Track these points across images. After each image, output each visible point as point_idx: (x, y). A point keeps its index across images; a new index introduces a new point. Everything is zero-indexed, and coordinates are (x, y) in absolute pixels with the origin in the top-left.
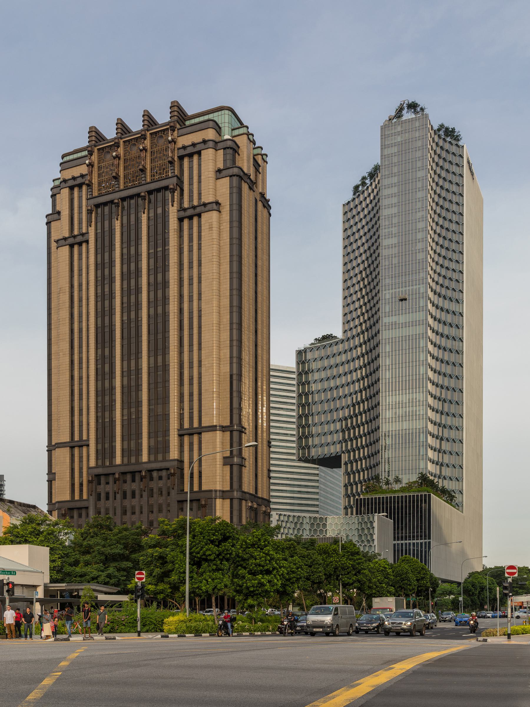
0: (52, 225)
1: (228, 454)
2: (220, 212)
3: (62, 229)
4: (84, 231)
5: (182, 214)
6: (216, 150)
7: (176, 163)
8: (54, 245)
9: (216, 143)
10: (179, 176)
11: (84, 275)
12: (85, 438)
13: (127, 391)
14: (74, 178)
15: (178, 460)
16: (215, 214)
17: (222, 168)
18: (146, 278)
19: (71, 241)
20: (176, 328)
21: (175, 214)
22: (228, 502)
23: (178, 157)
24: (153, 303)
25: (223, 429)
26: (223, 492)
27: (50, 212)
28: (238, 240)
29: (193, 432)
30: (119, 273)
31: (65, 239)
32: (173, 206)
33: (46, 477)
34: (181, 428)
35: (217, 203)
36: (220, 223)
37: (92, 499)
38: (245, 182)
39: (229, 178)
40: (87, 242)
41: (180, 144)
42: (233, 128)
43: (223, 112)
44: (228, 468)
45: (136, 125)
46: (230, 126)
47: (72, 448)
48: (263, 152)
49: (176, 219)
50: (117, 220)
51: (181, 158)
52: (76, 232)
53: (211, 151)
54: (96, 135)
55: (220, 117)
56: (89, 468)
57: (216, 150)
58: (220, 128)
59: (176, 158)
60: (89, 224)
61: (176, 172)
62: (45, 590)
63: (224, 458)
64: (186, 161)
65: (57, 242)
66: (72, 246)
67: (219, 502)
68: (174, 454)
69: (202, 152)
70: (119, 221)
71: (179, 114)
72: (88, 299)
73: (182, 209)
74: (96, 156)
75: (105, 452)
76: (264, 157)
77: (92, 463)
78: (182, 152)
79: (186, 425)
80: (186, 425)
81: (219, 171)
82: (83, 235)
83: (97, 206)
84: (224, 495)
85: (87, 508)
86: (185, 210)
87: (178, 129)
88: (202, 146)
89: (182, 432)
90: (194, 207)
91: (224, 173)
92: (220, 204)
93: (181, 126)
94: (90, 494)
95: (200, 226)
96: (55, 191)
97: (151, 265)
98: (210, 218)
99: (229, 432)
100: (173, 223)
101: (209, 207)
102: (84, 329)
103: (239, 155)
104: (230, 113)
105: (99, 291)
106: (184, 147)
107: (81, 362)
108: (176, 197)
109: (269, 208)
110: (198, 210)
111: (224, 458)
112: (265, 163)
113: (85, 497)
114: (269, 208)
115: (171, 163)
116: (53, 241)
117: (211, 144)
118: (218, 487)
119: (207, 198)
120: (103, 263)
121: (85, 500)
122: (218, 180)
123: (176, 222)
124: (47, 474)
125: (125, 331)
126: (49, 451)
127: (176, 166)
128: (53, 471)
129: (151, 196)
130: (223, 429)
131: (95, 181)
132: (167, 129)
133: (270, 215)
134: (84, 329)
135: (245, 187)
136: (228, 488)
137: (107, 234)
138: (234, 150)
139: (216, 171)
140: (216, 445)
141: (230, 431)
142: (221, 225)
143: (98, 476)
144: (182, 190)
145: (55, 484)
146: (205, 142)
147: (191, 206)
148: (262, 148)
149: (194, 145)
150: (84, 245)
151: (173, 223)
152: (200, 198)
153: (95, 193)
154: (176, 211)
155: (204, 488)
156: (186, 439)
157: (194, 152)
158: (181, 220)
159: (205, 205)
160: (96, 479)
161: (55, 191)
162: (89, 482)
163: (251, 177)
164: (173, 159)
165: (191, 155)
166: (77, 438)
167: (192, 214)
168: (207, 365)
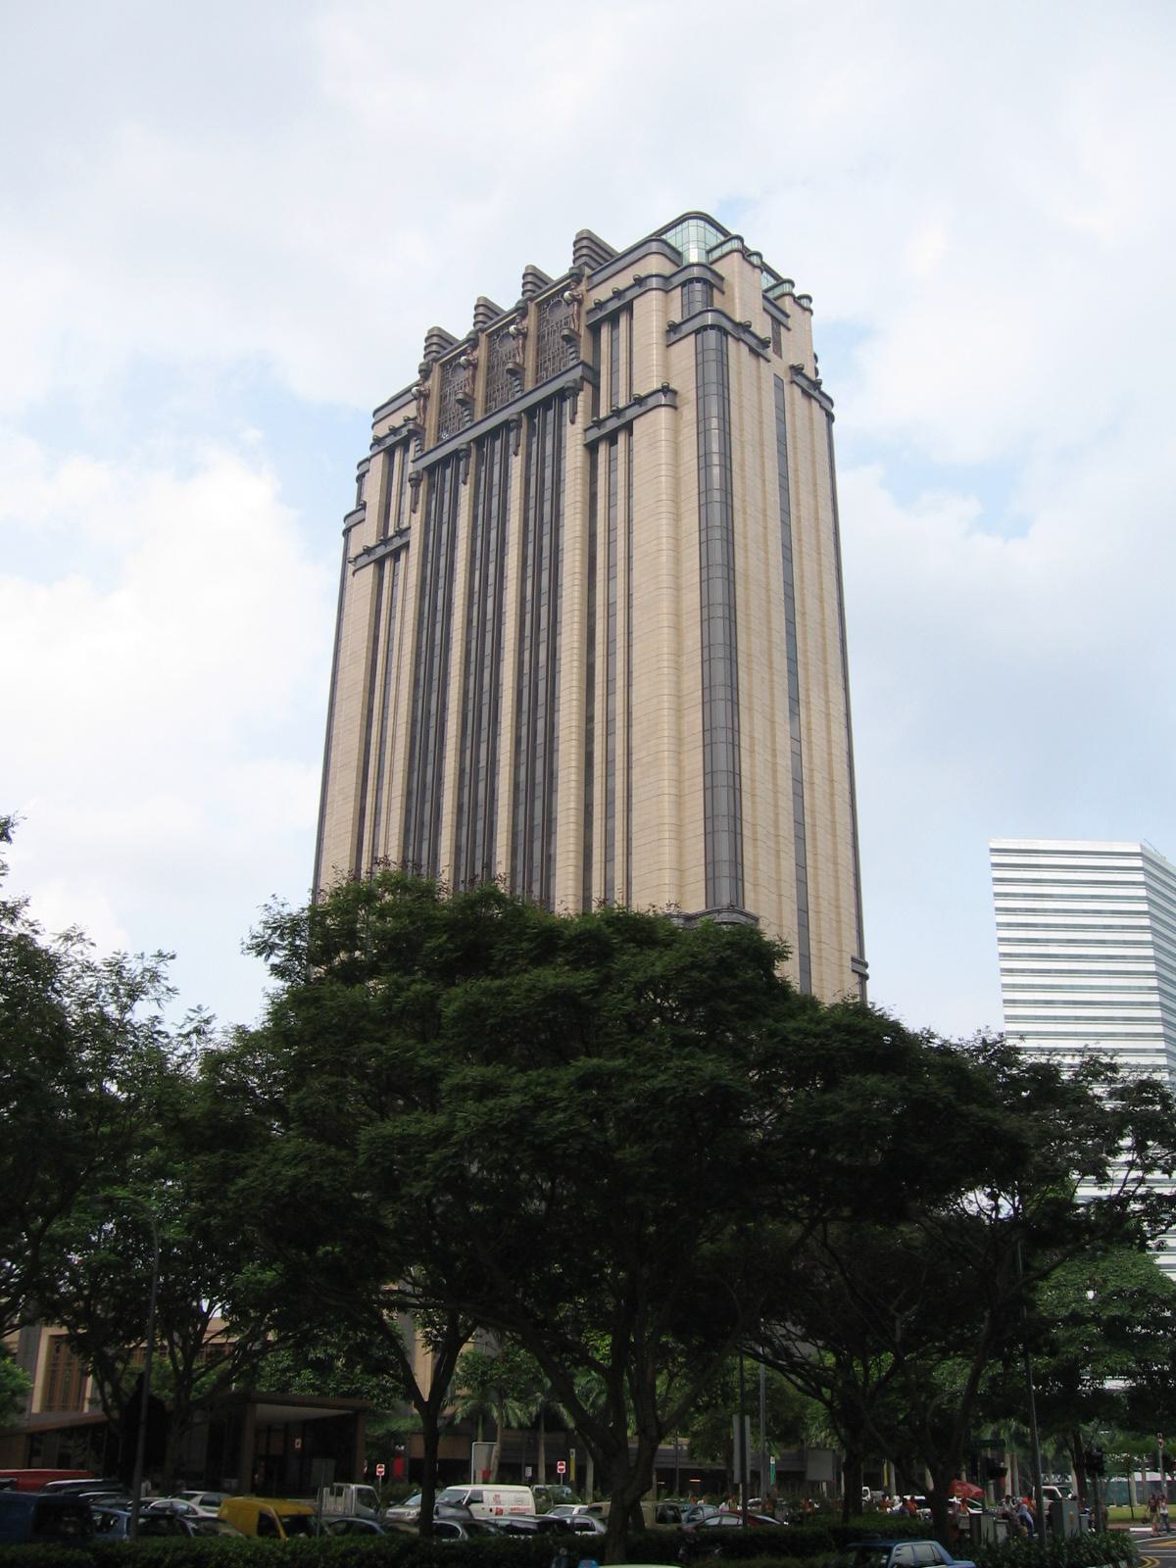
0: (375, 539)
3: (367, 535)
5: (594, 434)
6: (667, 292)
7: (582, 339)
14: (394, 431)
19: (381, 551)
21: (579, 436)
31: (368, 551)
32: (573, 422)
35: (666, 390)
36: (676, 431)
38: (738, 340)
42: (708, 248)
43: (685, 224)
45: (508, 298)
46: (702, 245)
47: (380, 563)
48: (797, 292)
49: (580, 448)
51: (595, 329)
54: (437, 341)
55: (679, 235)
57: (667, 292)
59: (583, 332)
61: (582, 355)
62: (501, 1481)
66: (380, 563)
70: (468, 486)
71: (591, 252)
76: (804, 302)
81: (673, 328)
83: (431, 469)
87: (589, 277)
88: (637, 291)
91: (686, 328)
92: (675, 393)
93: (593, 269)
96: (364, 468)
98: (653, 427)
101: (651, 402)
102: (619, 836)
104: (701, 223)
106: (600, 305)
108: (580, 404)
109: (826, 404)
112: (807, 313)
114: (826, 404)
115: (571, 340)
117: (654, 282)
119: (648, 382)
123: (579, 453)
133: (830, 417)
134: (619, 836)
138: (705, 281)
144: (596, 388)
146: (639, 281)
148: (793, 285)
149: (618, 294)
153: (430, 444)
157: (619, 310)
158: (591, 448)
159: (640, 401)
163: (756, 329)
165: (611, 439)
167: (611, 432)
168: (644, 760)
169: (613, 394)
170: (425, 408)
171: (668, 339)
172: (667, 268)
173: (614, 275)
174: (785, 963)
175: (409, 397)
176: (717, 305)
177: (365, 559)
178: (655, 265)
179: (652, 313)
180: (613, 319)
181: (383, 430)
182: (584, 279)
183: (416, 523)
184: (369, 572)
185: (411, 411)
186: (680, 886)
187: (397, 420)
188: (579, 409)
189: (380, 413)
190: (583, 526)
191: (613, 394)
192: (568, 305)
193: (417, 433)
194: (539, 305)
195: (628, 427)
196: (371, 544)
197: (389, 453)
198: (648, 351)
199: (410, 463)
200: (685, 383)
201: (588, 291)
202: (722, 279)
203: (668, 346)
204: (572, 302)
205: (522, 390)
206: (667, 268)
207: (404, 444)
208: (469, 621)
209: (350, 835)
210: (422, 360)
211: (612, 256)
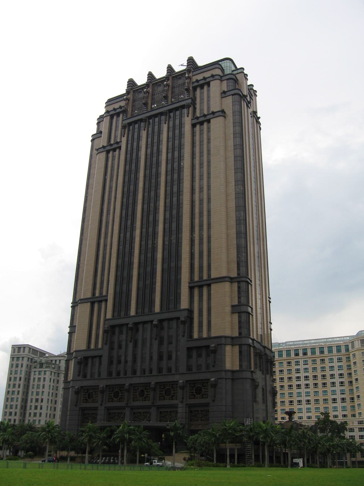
1: (236, 303)
2: (225, 117)
3: (103, 141)
4: (119, 140)
5: (195, 121)
8: (95, 152)
9: (221, 77)
10: (193, 98)
11: (108, 250)
12: (104, 294)
13: (146, 214)
14: (115, 109)
15: (188, 310)
16: (221, 119)
17: (226, 90)
18: (166, 133)
20: (188, 229)
22: (237, 349)
23: (192, 87)
24: (167, 232)
25: (231, 280)
26: (232, 338)
27: (95, 132)
28: (239, 127)
29: (202, 285)
30: (143, 176)
31: (104, 147)
32: (188, 116)
33: (68, 330)
34: (191, 280)
35: (223, 111)
37: (107, 347)
39: (231, 96)
40: (120, 148)
41: (194, 79)
43: (225, 61)
44: (236, 316)
47: (108, 152)
49: (187, 287)
50: (144, 130)
51: (195, 89)
52: (112, 142)
53: (218, 82)
54: (131, 83)
56: (106, 320)
58: (224, 70)
59: (191, 88)
60: (122, 135)
63: (233, 306)
64: (198, 90)
65: (97, 150)
66: (108, 152)
67: (228, 348)
68: (184, 304)
69: (212, 285)
70: (146, 131)
72: (115, 198)
73: (195, 117)
74: (132, 95)
75: (121, 302)
77: (109, 315)
78: (196, 84)
79: (196, 278)
80: (196, 278)
81: (224, 92)
82: (117, 143)
83: (130, 124)
84: (233, 341)
85: (100, 357)
86: (197, 118)
87: (193, 72)
88: (212, 116)
89: (192, 285)
90: (205, 116)
91: (228, 94)
94: (105, 343)
95: (209, 295)
97: (168, 168)
98: (216, 123)
99: (238, 347)
100: (187, 128)
103: (238, 84)
105: (126, 189)
106: (197, 81)
107: (108, 210)
108: (186, 328)
110: (208, 117)
111: (233, 306)
113: (100, 346)
116: (94, 149)
118: (228, 333)
119: (215, 108)
120: (130, 170)
121: (100, 349)
122: (223, 99)
124: (69, 327)
125: (147, 183)
126: (73, 307)
127: (191, 94)
128: (74, 324)
129: (171, 114)
130: (231, 280)
131: (130, 110)
132: (185, 73)
135: (244, 104)
136: (236, 334)
137: (135, 151)
139: (222, 93)
140: (223, 296)
141: (239, 345)
142: (227, 171)
143: (113, 327)
144: (195, 109)
145: (75, 336)
146: (213, 76)
147: (202, 115)
149: (205, 79)
150: (103, 304)
151: (187, 128)
152: (209, 108)
153: (129, 116)
154: (190, 119)
155: (213, 335)
156: (196, 291)
158: (194, 126)
159: (213, 113)
160: (111, 330)
161: (101, 119)
162: (105, 332)
164: (189, 88)
165: (201, 123)
166: (97, 294)
169: (201, 109)
170: (128, 104)
171: (222, 96)
172: (221, 74)
173: (112, 104)
174: (284, 149)
175: (122, 99)
176: (237, 87)
177: (102, 150)
178: (218, 72)
179: (216, 87)
180: (202, 87)
181: (111, 108)
182: (191, 72)
183: (124, 140)
184: (104, 155)
185: (123, 104)
186: (232, 328)
187: (116, 106)
188: (190, 112)
189: (110, 102)
190: (94, 265)
191: (201, 109)
192: (165, 86)
193: (125, 112)
194: (153, 84)
195: (209, 121)
196: (105, 145)
197: (112, 117)
198: (213, 98)
199: (120, 121)
200: (229, 112)
201: (193, 76)
202: (238, 80)
203: (222, 98)
204: (188, 78)
205: (168, 104)
206: (221, 74)
207: (118, 115)
208: (122, 203)
209: (94, 256)
210: (126, 88)
211: (155, 79)
